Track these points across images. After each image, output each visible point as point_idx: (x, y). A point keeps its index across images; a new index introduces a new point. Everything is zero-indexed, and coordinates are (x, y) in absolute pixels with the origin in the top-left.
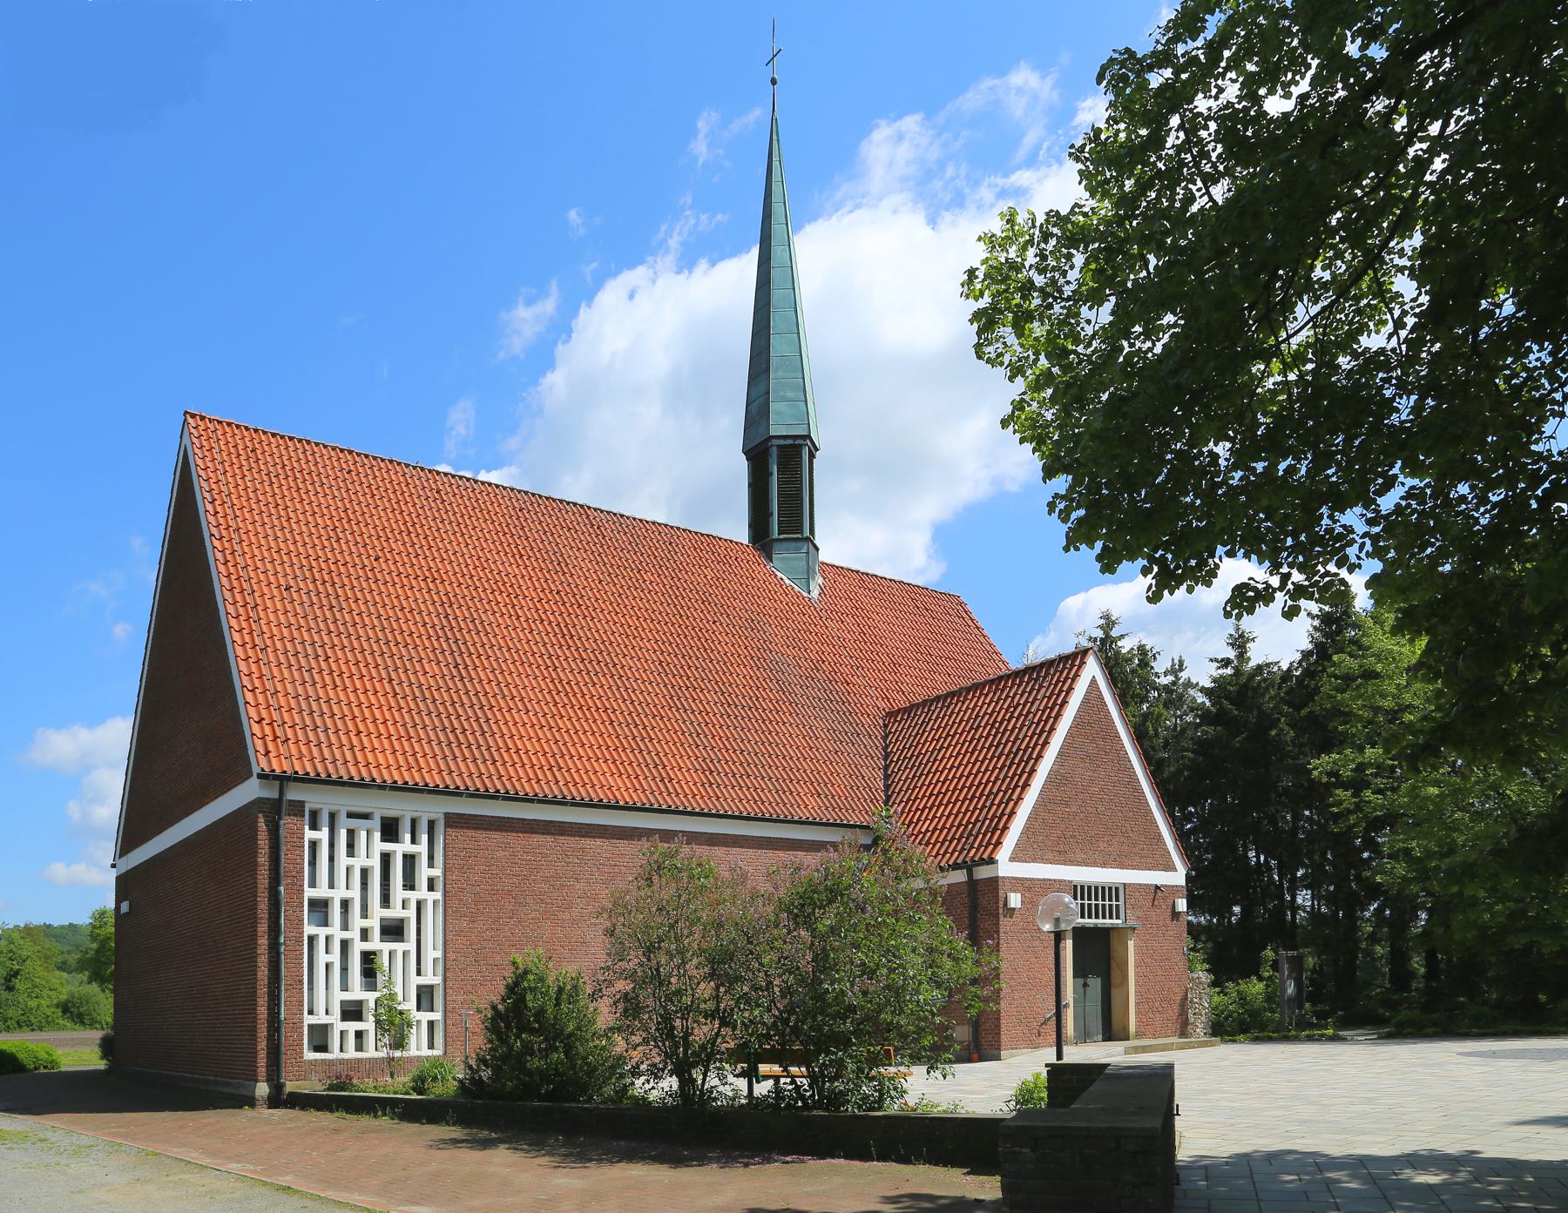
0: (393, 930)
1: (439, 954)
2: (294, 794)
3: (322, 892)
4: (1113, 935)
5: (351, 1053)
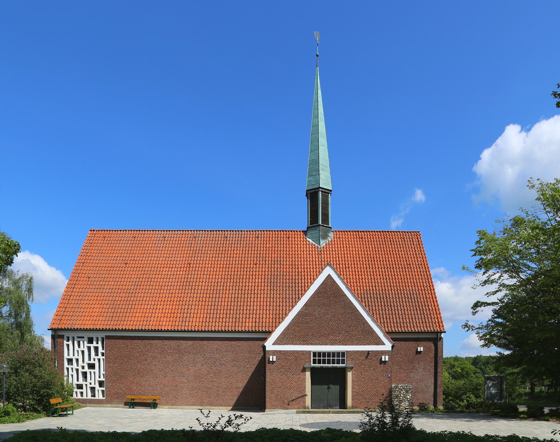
0: (92, 366)
1: (104, 373)
2: (61, 333)
3: (71, 356)
4: (335, 389)
5: (79, 396)
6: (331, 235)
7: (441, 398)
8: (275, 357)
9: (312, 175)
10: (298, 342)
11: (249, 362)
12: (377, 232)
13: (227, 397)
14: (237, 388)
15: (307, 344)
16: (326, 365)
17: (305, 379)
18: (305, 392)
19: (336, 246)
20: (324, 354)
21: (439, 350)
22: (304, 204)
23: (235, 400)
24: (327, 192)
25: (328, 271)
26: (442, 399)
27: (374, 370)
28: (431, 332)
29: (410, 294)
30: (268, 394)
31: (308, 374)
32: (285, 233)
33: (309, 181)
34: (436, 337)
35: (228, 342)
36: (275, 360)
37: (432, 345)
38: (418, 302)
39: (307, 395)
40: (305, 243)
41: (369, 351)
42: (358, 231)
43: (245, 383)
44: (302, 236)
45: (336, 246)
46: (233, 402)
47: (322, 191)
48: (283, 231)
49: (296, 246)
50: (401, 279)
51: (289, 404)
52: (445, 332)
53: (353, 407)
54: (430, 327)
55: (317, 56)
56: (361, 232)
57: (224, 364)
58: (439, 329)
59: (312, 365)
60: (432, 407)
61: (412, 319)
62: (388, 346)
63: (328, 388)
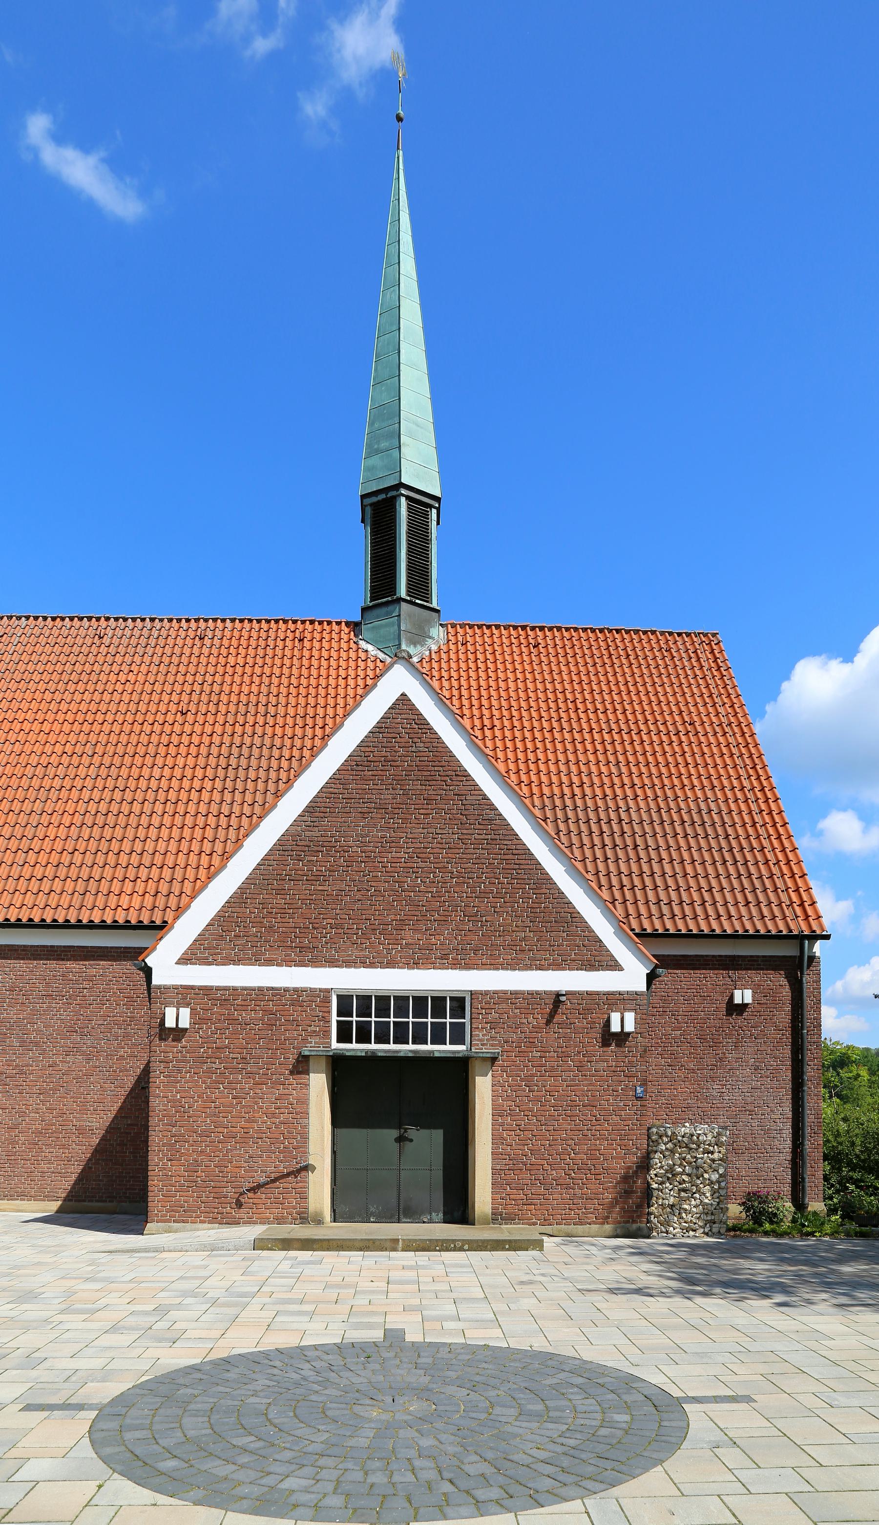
4: (428, 1143)
6: (438, 633)
7: (816, 1170)
8: (185, 1013)
9: (378, 452)
10: (280, 954)
11: (126, 1036)
12: (585, 630)
13: (44, 1166)
14: (81, 1131)
15: (315, 962)
16: (392, 1046)
17: (304, 1102)
18: (306, 1153)
19: (453, 665)
20: (383, 1001)
21: (808, 1002)
22: (359, 540)
23: (74, 1177)
24: (422, 504)
25: (398, 682)
26: (820, 1174)
27: (580, 1067)
28: (779, 937)
29: (700, 811)
30: (157, 1160)
31: (318, 1084)
32: (291, 626)
33: (368, 469)
34: (795, 952)
35: (53, 964)
36: (184, 1023)
37: (784, 981)
38: (727, 836)
39: (313, 1168)
40: (353, 655)
41: (558, 995)
42: (524, 628)
43: (111, 1116)
44: (345, 637)
45: (453, 665)
46: (66, 1185)
47: (408, 498)
48: (285, 622)
49: (324, 663)
50: (667, 765)
51: (239, 1204)
52: (827, 937)
53: (497, 1217)
54: (774, 918)
55: (399, 119)
56: (533, 628)
57: (37, 1044)
58: (804, 927)
59: (335, 1045)
60: (788, 1206)
61: (710, 890)
62: (631, 974)
63: (401, 1139)
